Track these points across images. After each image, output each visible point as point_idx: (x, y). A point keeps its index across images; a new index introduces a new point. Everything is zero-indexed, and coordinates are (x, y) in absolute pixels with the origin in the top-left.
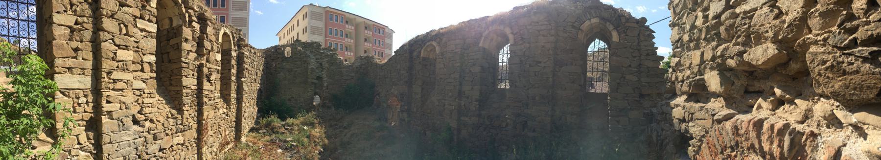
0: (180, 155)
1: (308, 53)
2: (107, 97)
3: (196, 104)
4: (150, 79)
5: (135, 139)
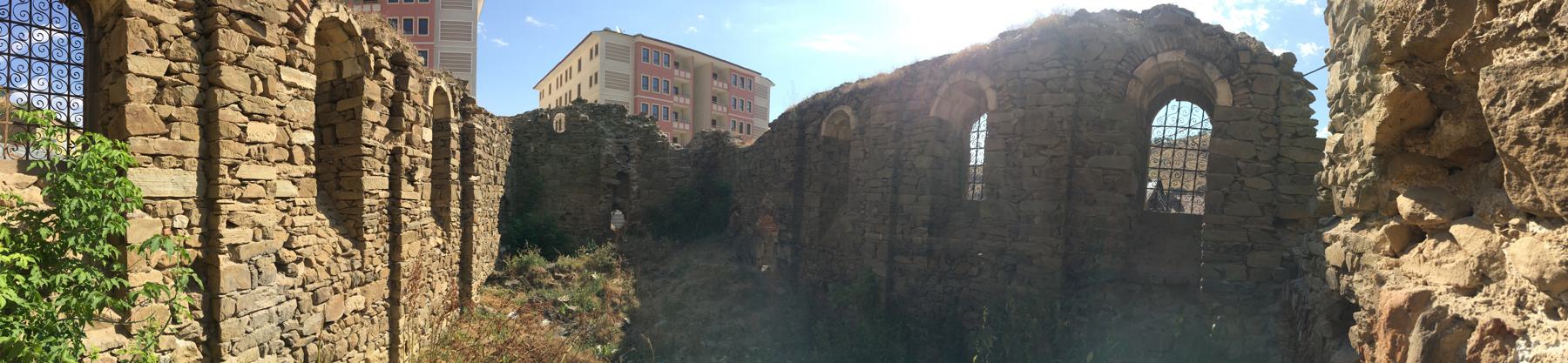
0: (358, 336)
1: (601, 125)
2: (228, 215)
3: (387, 227)
4: (305, 177)
5: (279, 303)
